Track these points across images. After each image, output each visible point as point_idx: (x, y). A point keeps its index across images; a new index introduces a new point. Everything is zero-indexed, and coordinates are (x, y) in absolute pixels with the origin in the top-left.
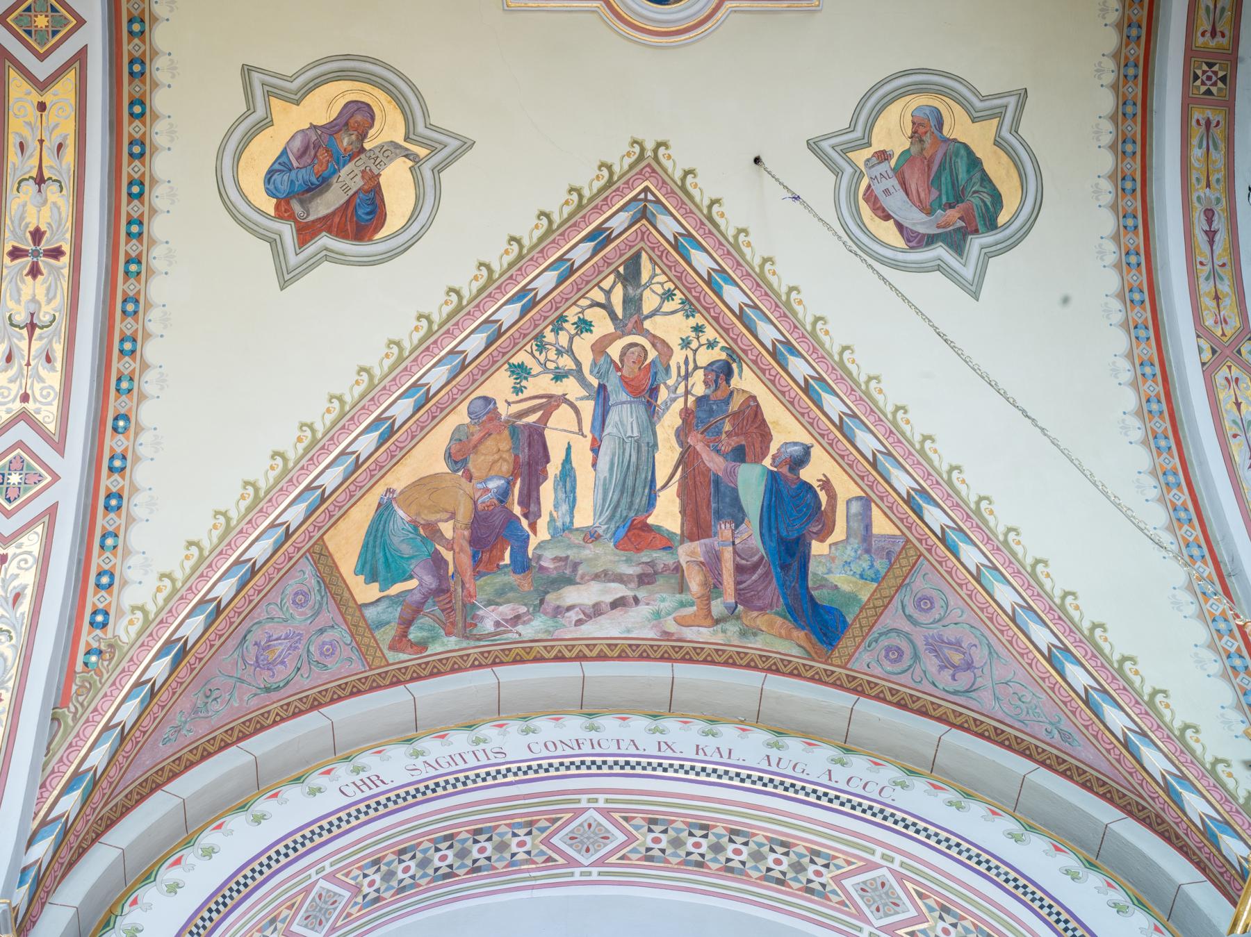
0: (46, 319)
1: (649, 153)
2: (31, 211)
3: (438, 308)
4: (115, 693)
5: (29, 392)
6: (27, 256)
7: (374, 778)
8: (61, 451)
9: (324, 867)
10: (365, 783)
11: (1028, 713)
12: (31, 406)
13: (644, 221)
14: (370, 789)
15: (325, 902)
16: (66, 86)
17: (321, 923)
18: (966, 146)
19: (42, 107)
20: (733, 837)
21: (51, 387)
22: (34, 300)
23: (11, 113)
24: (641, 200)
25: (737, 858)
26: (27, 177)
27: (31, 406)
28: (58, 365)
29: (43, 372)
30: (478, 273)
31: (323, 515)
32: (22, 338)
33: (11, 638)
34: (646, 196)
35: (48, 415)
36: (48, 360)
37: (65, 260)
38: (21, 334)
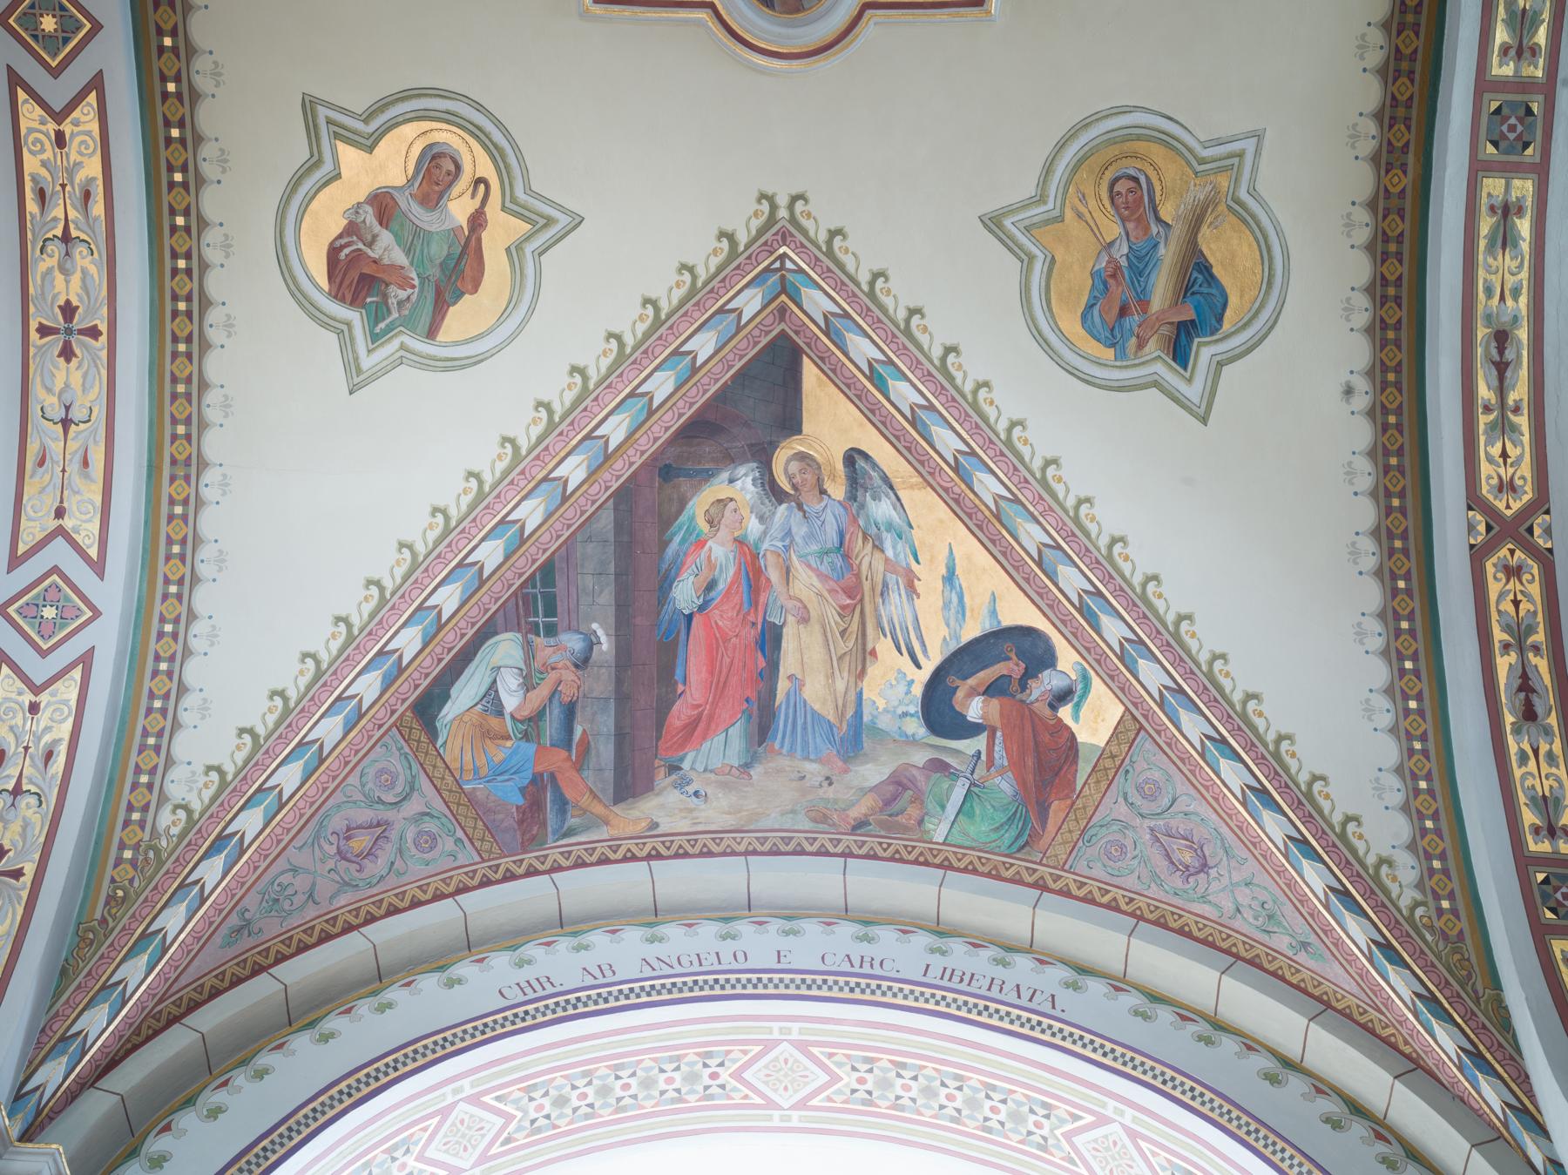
1: (783, 213)
2: (76, 379)
3: (561, 392)
4: (90, 984)
6: (66, 321)
7: (543, 980)
9: (472, 1087)
12: (28, 697)
13: (783, 298)
15: (469, 1128)
17: (465, 1149)
18: (852, 449)
19: (60, 140)
20: (990, 1093)
21: (33, 153)
24: (777, 270)
25: (995, 1117)
27: (28, 697)
30: (502, 451)
31: (143, 915)
32: (57, 439)
34: (783, 264)
37: (103, 339)
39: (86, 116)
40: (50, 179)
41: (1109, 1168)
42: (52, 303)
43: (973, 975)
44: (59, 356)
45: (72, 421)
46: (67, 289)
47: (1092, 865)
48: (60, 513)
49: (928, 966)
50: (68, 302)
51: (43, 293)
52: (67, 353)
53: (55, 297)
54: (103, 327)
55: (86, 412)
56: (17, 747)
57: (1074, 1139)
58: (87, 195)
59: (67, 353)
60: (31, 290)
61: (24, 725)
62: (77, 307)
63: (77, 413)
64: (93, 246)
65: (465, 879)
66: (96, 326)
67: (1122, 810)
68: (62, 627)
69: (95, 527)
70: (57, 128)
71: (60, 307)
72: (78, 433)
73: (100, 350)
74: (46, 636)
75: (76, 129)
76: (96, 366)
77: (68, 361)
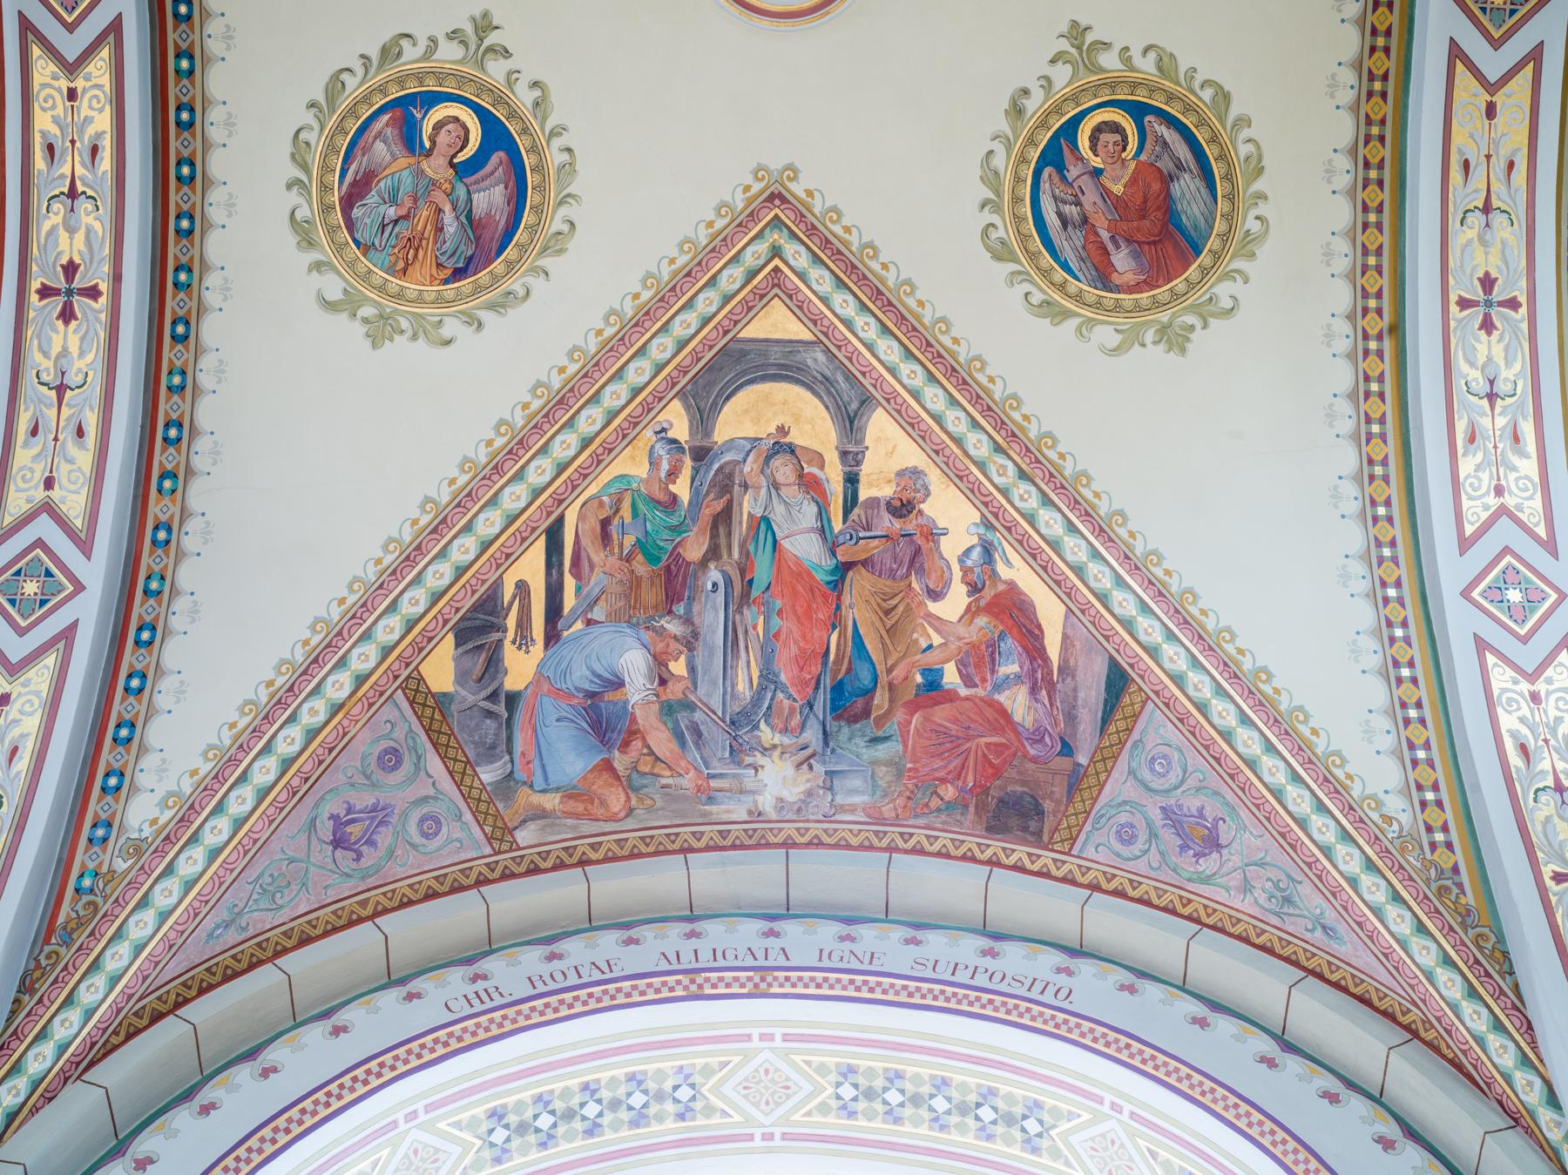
0: (56, 206)
2: (1498, 352)
5: (1503, 482)
8: (87, 553)
10: (479, 997)
11: (1015, 754)
14: (482, 1002)
16: (1476, 511)
21: (43, 109)
22: (71, 231)
23: (36, 105)
26: (77, 391)
27: (64, 84)
28: (38, 139)
29: (55, 130)
32: (49, 407)
33: (98, 209)
35: (73, 504)
36: (50, 148)
37: (1523, 310)
38: (1482, 407)
39: (99, 70)
40: (58, 133)
41: (1107, 1169)
42: (1471, 275)
43: (872, 954)
44: (1480, 329)
45: (1497, 395)
46: (69, 247)
47: (177, 789)
48: (49, 483)
49: (696, 951)
50: (1487, 274)
51: (1462, 266)
52: (1487, 325)
53: (1474, 268)
54: (1523, 299)
55: (1510, 386)
56: (1536, 741)
57: (1071, 1139)
58: (95, 150)
59: (1487, 325)
60: (1451, 263)
61: (1533, 715)
62: (1496, 279)
63: (1502, 387)
64: (99, 203)
65: (485, 870)
66: (1515, 297)
67: (1130, 791)
68: (1533, 610)
69: (1537, 503)
70: (1489, 99)
71: (62, 266)
72: (1505, 408)
73: (1522, 321)
74: (26, 615)
75: (89, 84)
76: (1518, 339)
77: (1489, 333)
